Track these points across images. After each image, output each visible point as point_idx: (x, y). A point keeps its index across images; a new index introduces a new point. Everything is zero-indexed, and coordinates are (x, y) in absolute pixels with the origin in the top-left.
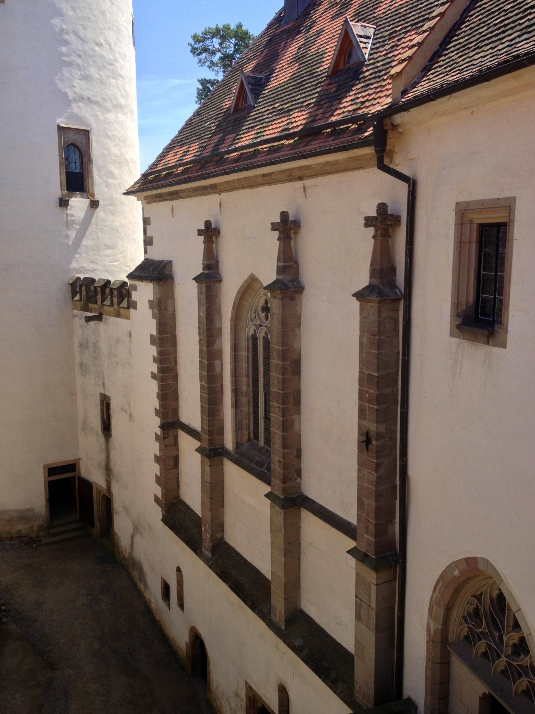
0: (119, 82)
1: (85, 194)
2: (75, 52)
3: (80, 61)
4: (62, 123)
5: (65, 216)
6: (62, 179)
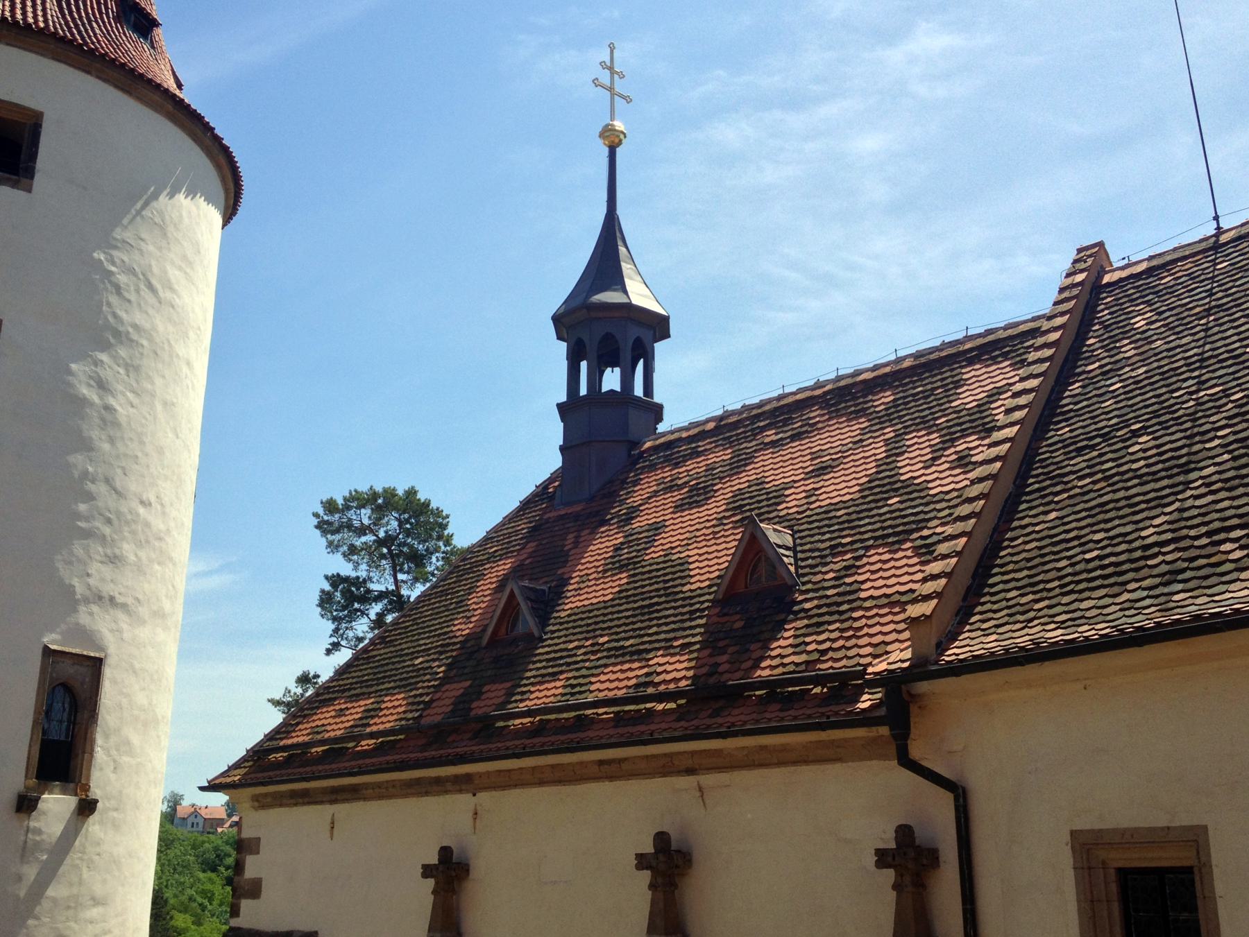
0: (167, 570)
1: (72, 785)
2: (101, 514)
3: (107, 530)
4: (53, 642)
5: (23, 832)
6: (32, 752)
